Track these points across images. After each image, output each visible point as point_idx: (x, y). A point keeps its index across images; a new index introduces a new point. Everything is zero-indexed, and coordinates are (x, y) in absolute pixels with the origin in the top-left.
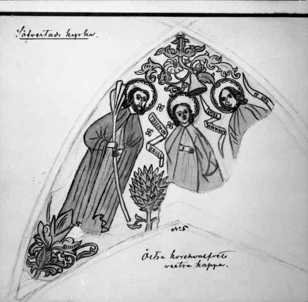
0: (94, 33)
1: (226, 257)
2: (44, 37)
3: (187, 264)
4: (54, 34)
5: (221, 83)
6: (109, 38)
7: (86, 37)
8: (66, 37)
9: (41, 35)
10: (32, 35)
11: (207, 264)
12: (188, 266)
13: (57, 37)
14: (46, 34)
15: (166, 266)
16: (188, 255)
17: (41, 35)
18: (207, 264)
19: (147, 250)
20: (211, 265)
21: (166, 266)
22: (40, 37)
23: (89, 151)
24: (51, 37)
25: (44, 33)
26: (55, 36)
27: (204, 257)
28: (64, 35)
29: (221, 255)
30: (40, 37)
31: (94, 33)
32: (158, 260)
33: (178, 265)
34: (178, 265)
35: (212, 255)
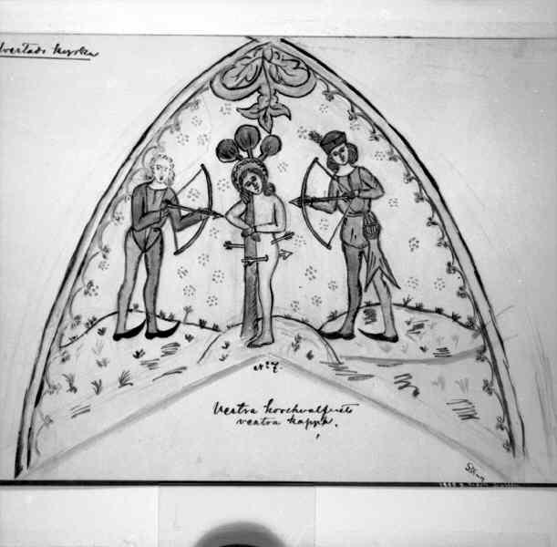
0: (97, 54)
1: (350, 411)
2: (22, 55)
3: (273, 420)
4: (35, 48)
5: (231, 166)
6: (520, 281)
7: (57, 55)
8: (53, 56)
9: (18, 50)
10: (5, 51)
11: (304, 420)
12: (275, 423)
13: (40, 54)
14: (24, 51)
15: (240, 421)
16: (285, 412)
17: (18, 50)
18: (304, 420)
19: (416, 393)
20: (311, 423)
21: (240, 421)
22: (17, 54)
23: (345, 316)
24: (31, 55)
25: (22, 48)
26: (36, 52)
27: (317, 411)
28: (50, 53)
29: (345, 409)
30: (17, 54)
31: (97, 54)
32: (317, 407)
33: (260, 421)
34: (260, 421)
35: (328, 409)
